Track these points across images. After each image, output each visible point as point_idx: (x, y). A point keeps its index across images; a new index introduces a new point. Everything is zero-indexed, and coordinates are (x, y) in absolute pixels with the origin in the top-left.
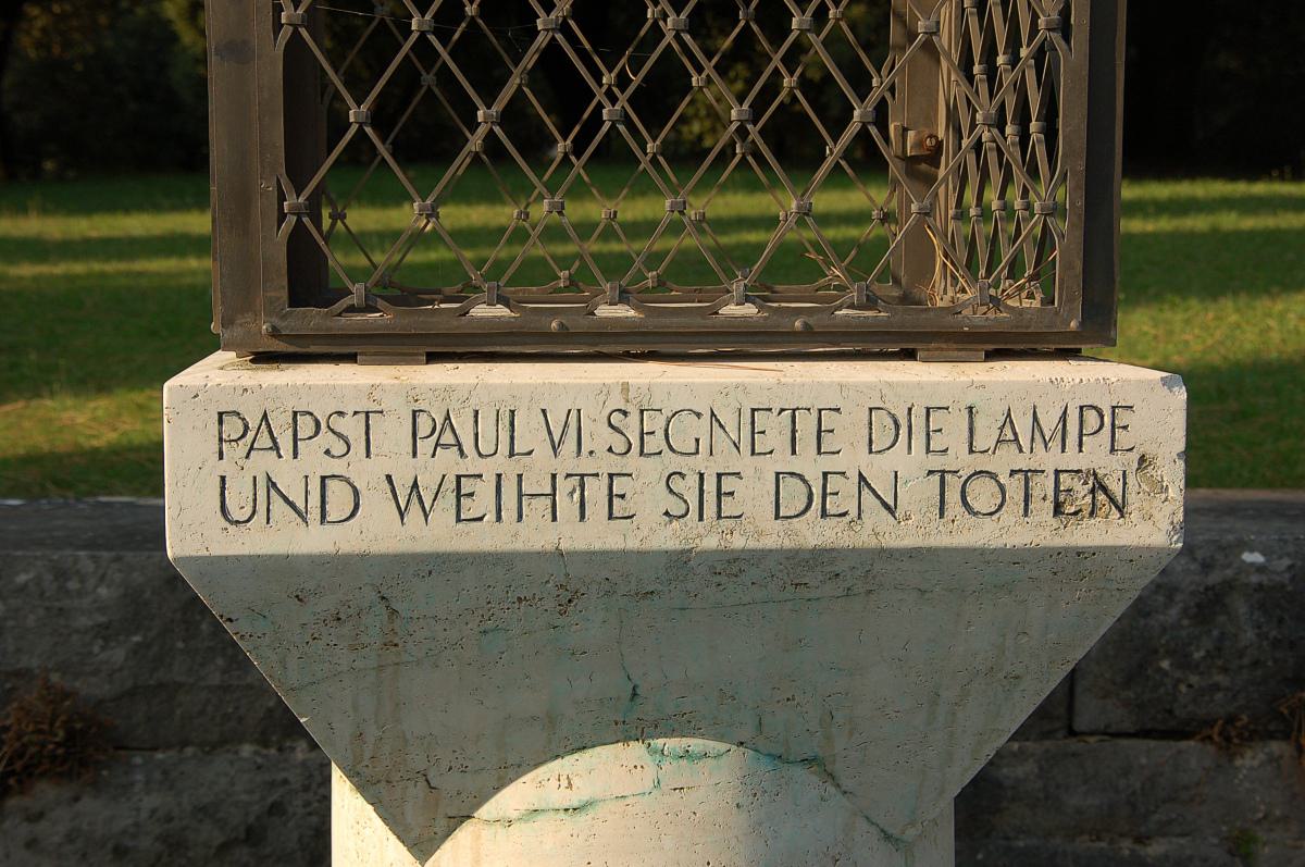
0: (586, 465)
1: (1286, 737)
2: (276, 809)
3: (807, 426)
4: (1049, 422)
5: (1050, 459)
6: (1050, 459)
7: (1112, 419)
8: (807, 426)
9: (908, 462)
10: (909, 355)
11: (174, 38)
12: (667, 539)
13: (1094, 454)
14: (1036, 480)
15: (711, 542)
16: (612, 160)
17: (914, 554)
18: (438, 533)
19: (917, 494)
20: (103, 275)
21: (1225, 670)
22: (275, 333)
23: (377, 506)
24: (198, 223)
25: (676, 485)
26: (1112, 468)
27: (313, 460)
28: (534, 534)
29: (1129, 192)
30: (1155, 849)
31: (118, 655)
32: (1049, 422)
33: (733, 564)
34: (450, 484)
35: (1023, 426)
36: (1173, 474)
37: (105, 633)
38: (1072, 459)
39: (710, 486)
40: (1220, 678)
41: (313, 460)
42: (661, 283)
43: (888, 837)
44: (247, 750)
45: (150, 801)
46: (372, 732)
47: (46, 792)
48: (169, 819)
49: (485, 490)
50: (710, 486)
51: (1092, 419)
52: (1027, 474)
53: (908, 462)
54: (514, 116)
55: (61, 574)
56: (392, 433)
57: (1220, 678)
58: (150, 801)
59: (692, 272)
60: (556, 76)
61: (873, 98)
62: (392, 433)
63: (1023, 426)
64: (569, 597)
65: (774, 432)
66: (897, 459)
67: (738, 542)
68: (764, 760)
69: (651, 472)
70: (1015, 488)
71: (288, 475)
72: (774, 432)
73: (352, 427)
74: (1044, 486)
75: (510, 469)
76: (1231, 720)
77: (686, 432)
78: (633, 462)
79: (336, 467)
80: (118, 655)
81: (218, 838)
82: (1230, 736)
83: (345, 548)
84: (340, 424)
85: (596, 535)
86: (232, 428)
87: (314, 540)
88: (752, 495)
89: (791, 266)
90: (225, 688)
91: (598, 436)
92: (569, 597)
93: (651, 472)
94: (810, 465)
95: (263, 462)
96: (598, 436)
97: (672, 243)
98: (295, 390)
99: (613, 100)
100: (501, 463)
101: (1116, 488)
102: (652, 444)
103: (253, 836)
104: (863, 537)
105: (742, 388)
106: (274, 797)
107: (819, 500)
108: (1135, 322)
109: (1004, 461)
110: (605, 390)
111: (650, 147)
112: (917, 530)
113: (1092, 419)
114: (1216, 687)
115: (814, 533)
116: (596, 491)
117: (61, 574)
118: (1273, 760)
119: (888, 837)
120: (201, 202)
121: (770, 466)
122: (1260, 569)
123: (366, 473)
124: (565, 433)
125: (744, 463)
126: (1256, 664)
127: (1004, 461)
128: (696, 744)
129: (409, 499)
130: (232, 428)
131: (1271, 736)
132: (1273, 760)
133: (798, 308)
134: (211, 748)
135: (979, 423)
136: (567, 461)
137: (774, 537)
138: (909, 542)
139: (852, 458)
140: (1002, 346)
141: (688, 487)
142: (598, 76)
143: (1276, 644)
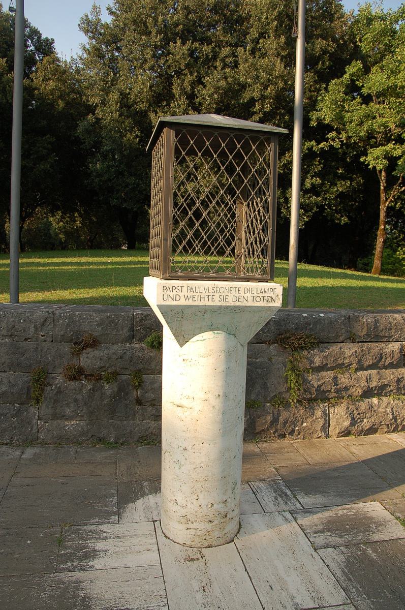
0: (209, 294)
1: (277, 343)
2: (125, 353)
3: (237, 290)
4: (266, 290)
5: (266, 295)
6: (266, 295)
7: (274, 290)
8: (237, 290)
9: (249, 295)
10: (248, 281)
11: (52, 224)
12: (219, 304)
13: (272, 295)
14: (265, 298)
15: (225, 305)
16: (221, 253)
17: (249, 306)
18: (190, 303)
19: (250, 299)
20: (55, 269)
21: (269, 333)
22: (169, 276)
23: (183, 299)
24: (7, 261)
25: (220, 297)
26: (274, 296)
27: (175, 293)
28: (202, 303)
29: (276, 261)
30: (258, 360)
31: (100, 329)
32: (266, 290)
33: (227, 307)
34: (192, 296)
35: (263, 291)
36: (281, 297)
37: (97, 325)
38: (269, 295)
39: (225, 297)
40: (269, 335)
41: (175, 293)
42: (203, 272)
43: (241, 345)
44: (119, 344)
45: (105, 352)
46: (178, 329)
47: (89, 350)
48: (108, 354)
49: (196, 297)
50: (225, 297)
51: (272, 290)
52: (264, 297)
53: (249, 295)
54: (184, 247)
55: (90, 316)
56: (185, 289)
57: (269, 335)
58: (105, 352)
59: (207, 270)
60: (190, 244)
61: (231, 247)
62: (185, 289)
63: (263, 291)
64: (206, 311)
65: (233, 291)
66: (248, 294)
67: (228, 305)
68: (227, 334)
69: (217, 295)
70: (262, 298)
71: (172, 294)
72: (233, 291)
73: (180, 288)
74: (265, 298)
75: (200, 294)
76: (270, 341)
77: (222, 290)
78: (215, 294)
79: (178, 294)
80: (100, 329)
81: (116, 357)
82: (270, 343)
83: (178, 304)
84: (178, 288)
85: (210, 303)
86: (165, 288)
87: (174, 303)
88: (230, 299)
89: (221, 269)
90: (116, 334)
91: (211, 290)
92: (206, 311)
93: (217, 295)
94: (237, 295)
95: (168, 293)
96: (211, 290)
97: (184, 265)
98: (174, 283)
99: (197, 246)
100: (199, 294)
101: (274, 299)
102: (218, 292)
103: (121, 357)
104: (243, 305)
105: (230, 285)
106: (124, 352)
107: (238, 299)
108: (275, 279)
109: (261, 295)
110: (212, 284)
111: (202, 252)
112: (250, 304)
113: (272, 290)
114: (268, 336)
115: (237, 304)
116: (210, 297)
117: (90, 316)
118: (275, 347)
119: (241, 345)
120: (7, 258)
121: (232, 295)
122: (275, 318)
123: (181, 294)
124: (207, 290)
125: (229, 294)
126: (273, 332)
127: (261, 295)
128: (219, 332)
129: (187, 298)
130: (165, 288)
131: (275, 343)
132: (275, 347)
133: (221, 275)
134: (114, 344)
135: (258, 290)
136: (207, 293)
137: (233, 304)
138: (249, 305)
139: (242, 294)
140: (260, 281)
141: (222, 297)
142: (195, 242)
143: (276, 329)
